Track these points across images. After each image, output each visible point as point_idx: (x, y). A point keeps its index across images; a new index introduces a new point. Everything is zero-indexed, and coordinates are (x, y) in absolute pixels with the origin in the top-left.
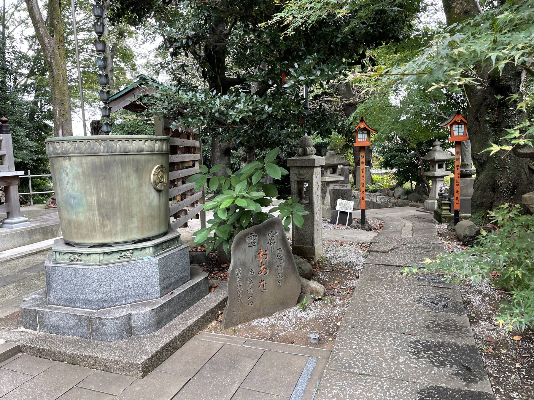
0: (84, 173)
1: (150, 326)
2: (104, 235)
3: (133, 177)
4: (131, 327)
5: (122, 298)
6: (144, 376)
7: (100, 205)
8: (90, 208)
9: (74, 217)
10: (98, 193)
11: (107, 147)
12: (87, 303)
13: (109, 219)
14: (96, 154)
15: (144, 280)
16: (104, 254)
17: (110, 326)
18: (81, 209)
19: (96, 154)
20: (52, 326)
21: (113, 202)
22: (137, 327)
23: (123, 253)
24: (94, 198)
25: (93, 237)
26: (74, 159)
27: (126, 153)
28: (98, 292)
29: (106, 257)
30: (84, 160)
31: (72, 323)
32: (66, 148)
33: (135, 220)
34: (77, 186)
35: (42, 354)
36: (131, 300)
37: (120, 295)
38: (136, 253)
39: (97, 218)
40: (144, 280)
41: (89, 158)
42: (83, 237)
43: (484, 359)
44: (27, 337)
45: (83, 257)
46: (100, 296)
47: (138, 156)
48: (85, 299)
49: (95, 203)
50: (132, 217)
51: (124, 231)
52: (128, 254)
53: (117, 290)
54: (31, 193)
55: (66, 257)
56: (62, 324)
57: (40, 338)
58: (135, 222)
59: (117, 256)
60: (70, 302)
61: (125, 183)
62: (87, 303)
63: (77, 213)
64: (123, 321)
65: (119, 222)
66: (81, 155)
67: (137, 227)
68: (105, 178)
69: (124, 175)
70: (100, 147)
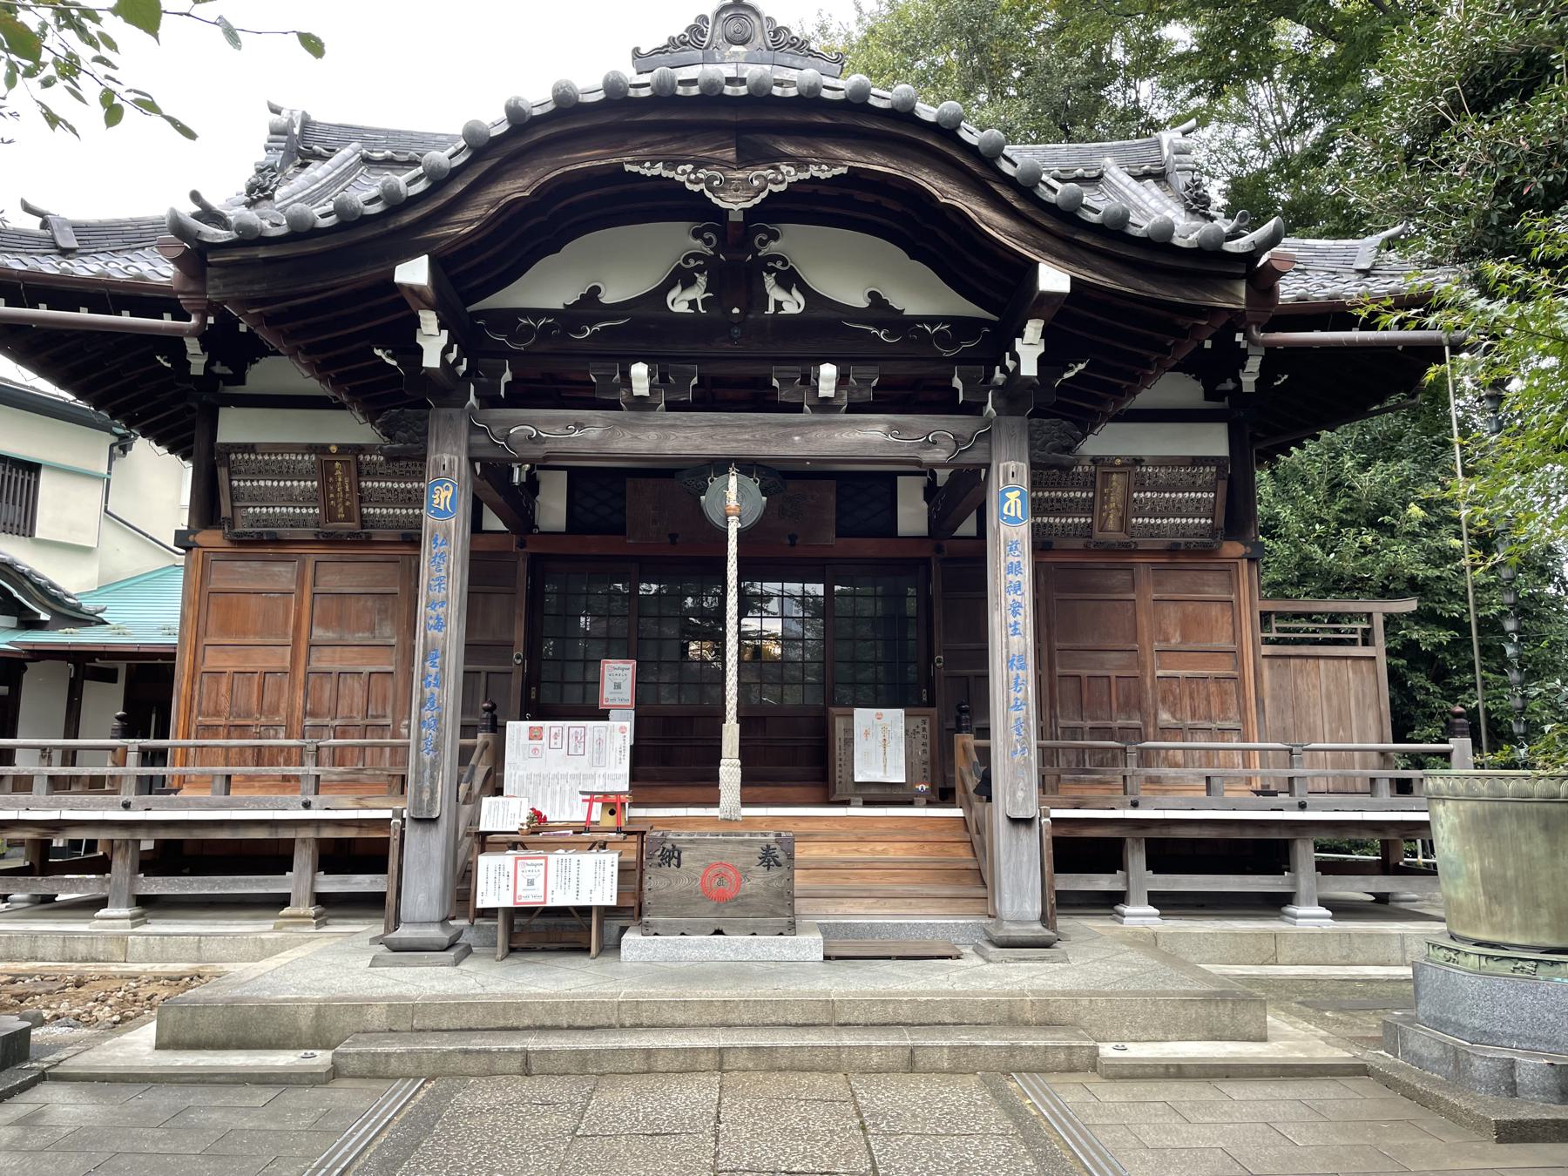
0: (1462, 826)
1: (1544, 1091)
2: (1494, 928)
3: (1539, 838)
4: (1514, 1082)
5: (1512, 1036)
6: (989, 799)
7: (1487, 878)
8: (1472, 882)
9: (1452, 893)
10: (1482, 859)
11: (1491, 787)
12: (1459, 1029)
13: (1500, 904)
14: (1476, 798)
15: (1551, 1016)
16: (1488, 957)
17: (1479, 1068)
18: (1460, 882)
19: (1476, 798)
20: (1415, 1054)
21: (1504, 877)
22: (1524, 1085)
23: (1520, 964)
24: (1476, 866)
25: (1476, 929)
26: (1449, 803)
27: (1525, 798)
28: (1473, 1014)
29: (1491, 963)
30: (1461, 806)
31: (1436, 1054)
32: (1438, 787)
33: (1544, 911)
34: (1453, 845)
35: (1389, 1082)
36: (1528, 1045)
37: (1509, 1030)
38: (1542, 968)
39: (1481, 899)
40: (1551, 1016)
41: (1468, 804)
42: (1464, 927)
43: (1339, 151)
44: (1381, 1061)
45: (1461, 957)
46: (1477, 1023)
47: (1548, 806)
48: (1457, 1023)
49: (1478, 874)
50: (1539, 906)
51: (1525, 928)
52: (1528, 966)
53: (1504, 1021)
54: (1257, 745)
55: (1443, 952)
56: (1425, 1052)
57: (1397, 1067)
58: (1545, 917)
59: (1510, 965)
60: (1440, 1024)
61: (1524, 848)
62: (1459, 1029)
63: (1456, 887)
64: (1500, 1066)
65: (1516, 909)
66: (1457, 798)
67: (1549, 925)
68: (1491, 837)
69: (1521, 834)
70: (1482, 787)
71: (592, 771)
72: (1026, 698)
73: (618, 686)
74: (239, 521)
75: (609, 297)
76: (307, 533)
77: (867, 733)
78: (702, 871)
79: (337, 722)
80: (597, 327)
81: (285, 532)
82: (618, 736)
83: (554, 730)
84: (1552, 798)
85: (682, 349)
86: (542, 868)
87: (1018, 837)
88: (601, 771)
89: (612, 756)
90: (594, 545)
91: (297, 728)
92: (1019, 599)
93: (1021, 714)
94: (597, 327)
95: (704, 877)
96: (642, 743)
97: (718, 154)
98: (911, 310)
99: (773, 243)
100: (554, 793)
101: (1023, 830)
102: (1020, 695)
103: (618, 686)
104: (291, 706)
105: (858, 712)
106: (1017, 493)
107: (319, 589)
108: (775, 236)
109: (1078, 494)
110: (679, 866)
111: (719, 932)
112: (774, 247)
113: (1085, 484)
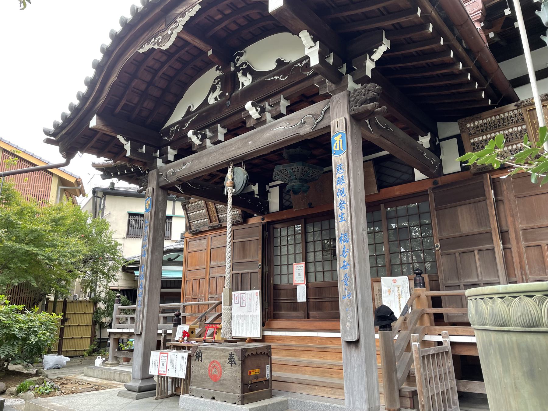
47: (529, 338)
71: (248, 314)
72: (349, 261)
73: (299, 275)
74: (192, 227)
75: (193, 109)
76: (206, 228)
77: (389, 291)
78: (209, 364)
79: (216, 296)
80: (189, 122)
81: (202, 229)
82: (255, 296)
83: (236, 295)
84: (532, 326)
85: (213, 120)
86: (166, 358)
87: (351, 353)
88: (251, 313)
89: (254, 307)
90: (286, 215)
91: (207, 299)
92: (343, 199)
93: (347, 271)
94: (189, 122)
95: (209, 367)
96: (311, 300)
97: (160, 28)
98: (294, 60)
99: (241, 58)
100: (236, 324)
101: (353, 349)
102: (346, 259)
103: (299, 275)
104: (206, 291)
105: (383, 279)
106: (340, 136)
107: (212, 247)
108: (241, 55)
109: (515, 129)
110: (201, 361)
111: (213, 398)
112: (243, 59)
113: (518, 121)
